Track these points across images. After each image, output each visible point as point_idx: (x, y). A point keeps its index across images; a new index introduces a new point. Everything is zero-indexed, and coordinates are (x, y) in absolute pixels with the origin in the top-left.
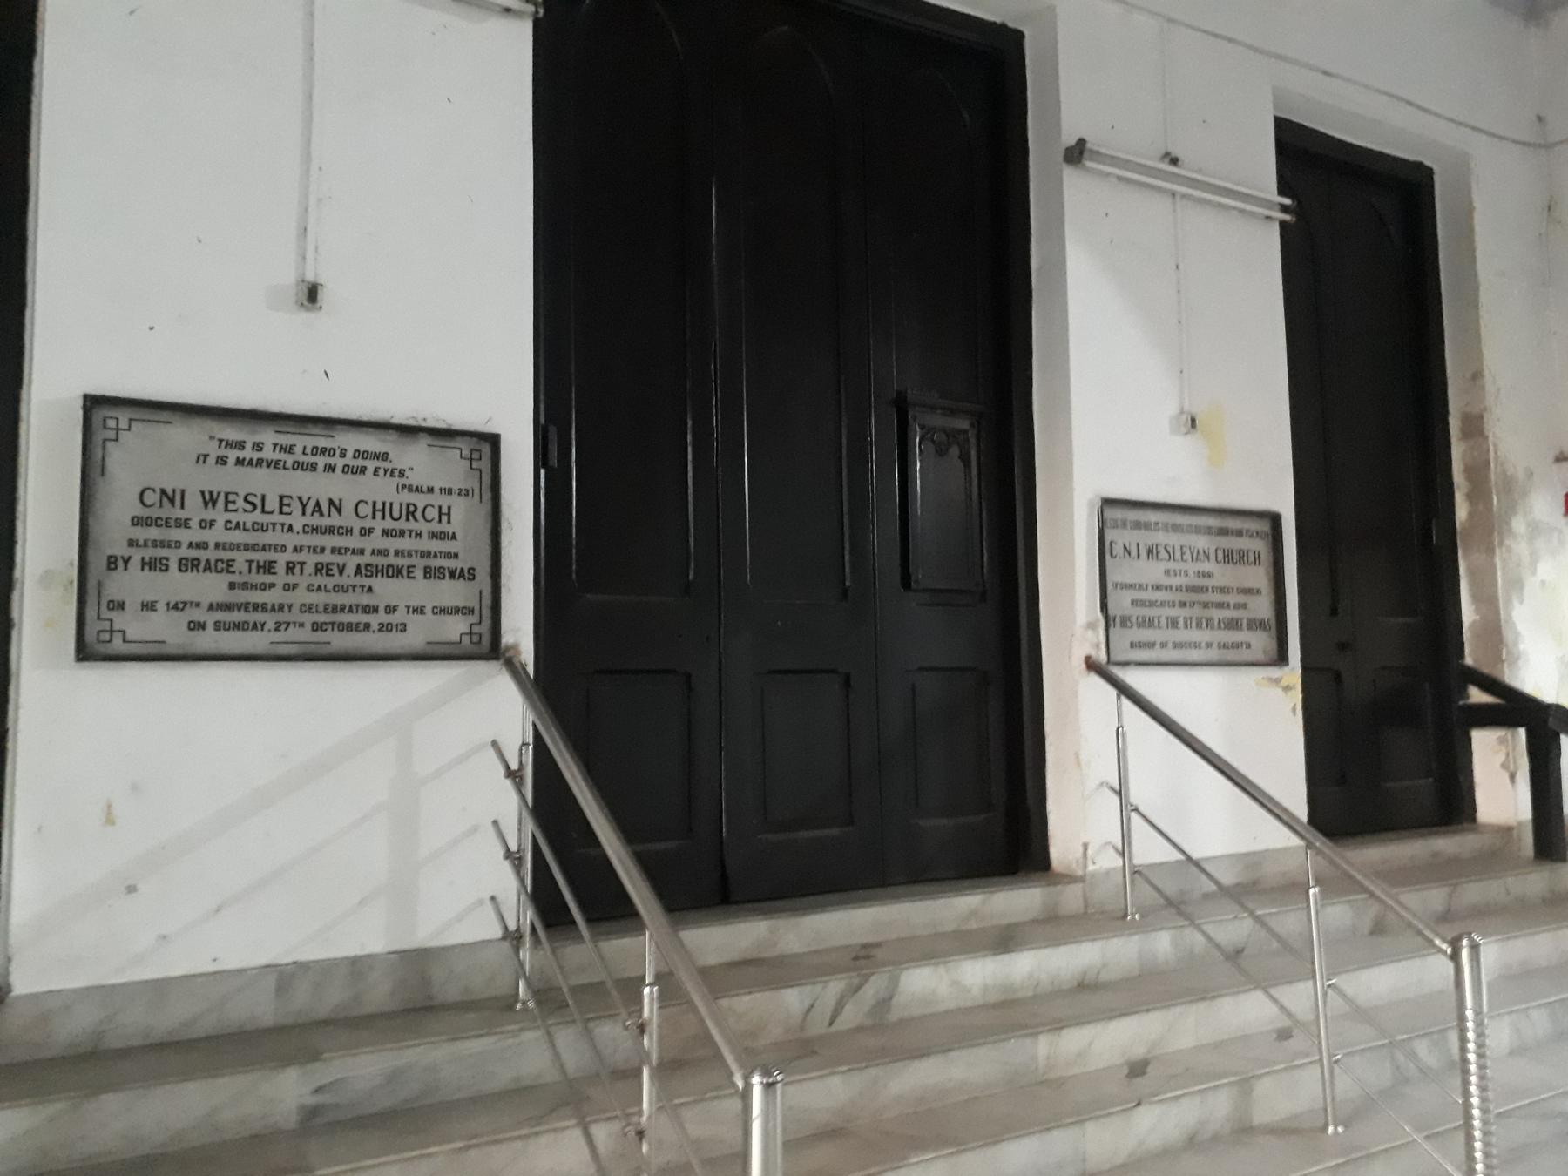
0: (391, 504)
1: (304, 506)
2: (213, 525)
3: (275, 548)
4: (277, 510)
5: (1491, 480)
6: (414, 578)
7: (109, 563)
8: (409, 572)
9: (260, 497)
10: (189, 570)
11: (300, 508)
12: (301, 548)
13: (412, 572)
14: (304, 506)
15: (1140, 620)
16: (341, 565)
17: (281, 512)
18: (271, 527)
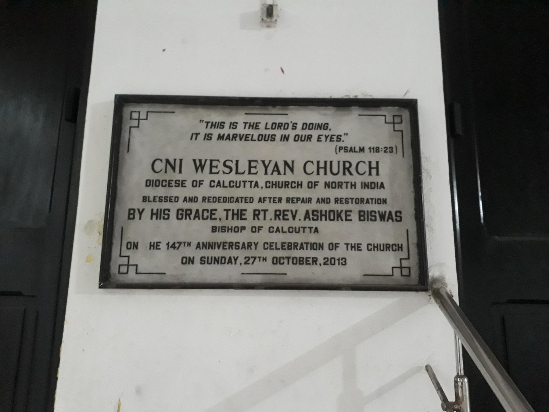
1: (266, 168)
4: (247, 172)
11: (264, 169)
14: (266, 168)
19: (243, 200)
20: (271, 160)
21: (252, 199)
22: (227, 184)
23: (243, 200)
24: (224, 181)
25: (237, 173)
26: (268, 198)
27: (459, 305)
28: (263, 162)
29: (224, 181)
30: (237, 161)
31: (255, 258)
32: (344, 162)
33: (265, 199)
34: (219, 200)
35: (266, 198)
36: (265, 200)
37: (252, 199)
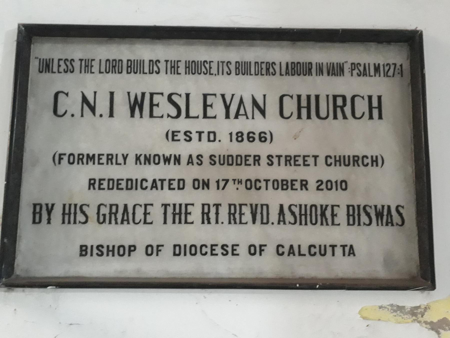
0: (369, 64)
1: (227, 108)
2: (263, 250)
3: (170, 184)
4: (201, 115)
5: (17, 91)
6: (238, 255)
7: (81, 250)
8: (233, 250)
9: (184, 96)
10: (44, 71)
11: (224, 111)
12: (190, 161)
13: (236, 250)
14: (227, 108)
15: (105, 210)
16: (125, 155)
17: (205, 116)
18: (329, 250)
19: (166, 184)
20: (233, 93)
21: (181, 182)
22: (304, 250)
23: (166, 184)
24: (299, 246)
25: (188, 116)
26: (311, 156)
27: (140, 104)
28: (223, 96)
29: (299, 246)
30: (188, 95)
31: (227, 181)
32: (335, 97)
33: (62, 156)
34: (118, 184)
35: (309, 156)
36: (62, 159)
37: (181, 182)
